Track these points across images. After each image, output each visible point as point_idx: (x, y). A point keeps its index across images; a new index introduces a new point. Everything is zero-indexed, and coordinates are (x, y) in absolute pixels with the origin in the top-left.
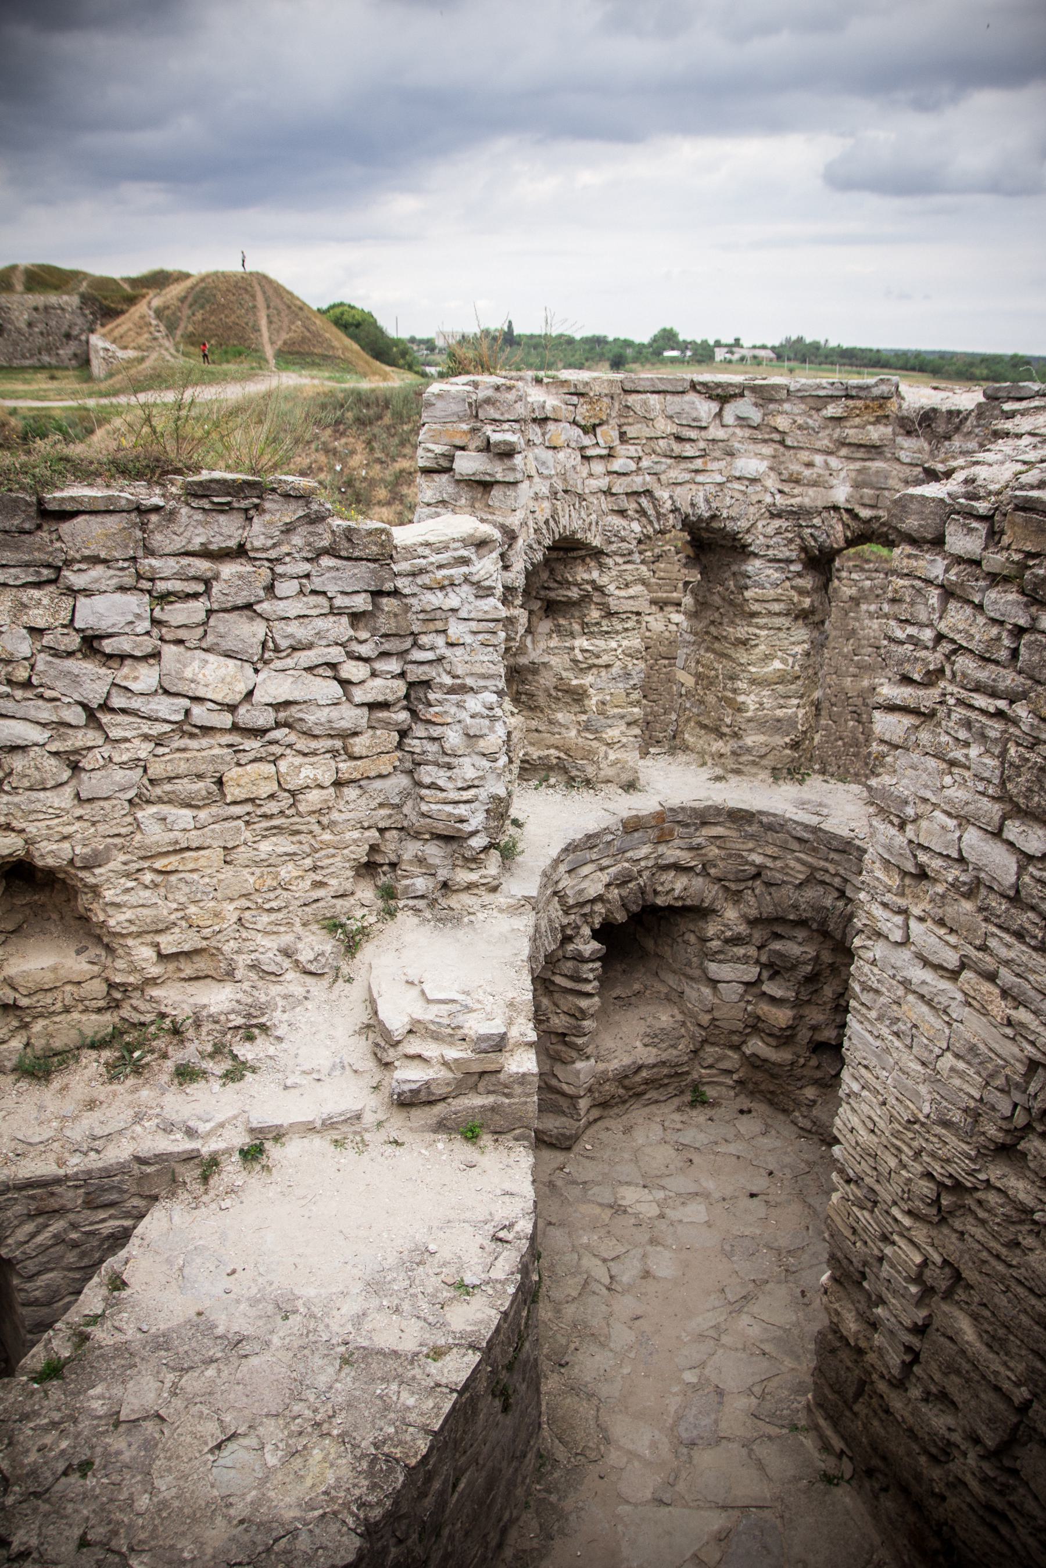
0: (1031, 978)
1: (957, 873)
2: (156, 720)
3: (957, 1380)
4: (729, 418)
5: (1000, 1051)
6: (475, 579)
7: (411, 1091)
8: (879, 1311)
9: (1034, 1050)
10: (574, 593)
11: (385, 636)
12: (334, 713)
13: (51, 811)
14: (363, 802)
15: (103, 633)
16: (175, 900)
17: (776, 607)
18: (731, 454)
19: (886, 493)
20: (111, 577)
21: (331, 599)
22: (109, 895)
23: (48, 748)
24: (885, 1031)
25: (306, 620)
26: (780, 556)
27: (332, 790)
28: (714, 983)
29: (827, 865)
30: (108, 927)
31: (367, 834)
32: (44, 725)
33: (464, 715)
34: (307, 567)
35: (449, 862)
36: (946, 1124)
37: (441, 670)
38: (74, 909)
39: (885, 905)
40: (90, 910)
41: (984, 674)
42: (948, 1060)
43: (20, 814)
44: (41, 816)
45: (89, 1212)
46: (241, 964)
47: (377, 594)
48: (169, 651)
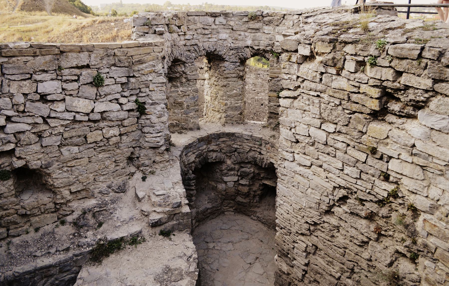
0: (332, 165)
1: (309, 140)
2: (65, 120)
3: (319, 275)
4: (217, 23)
5: (324, 186)
6: (156, 71)
7: (155, 222)
8: (294, 262)
9: (335, 184)
10: (178, 75)
11: (132, 89)
12: (118, 114)
13: (34, 151)
14: (128, 139)
15: (47, 94)
16: (74, 175)
17: (234, 75)
18: (218, 33)
19: (261, 42)
20: (49, 76)
21: (115, 79)
22: (54, 176)
23: (31, 131)
24: (290, 186)
25: (108, 86)
26: (234, 61)
27: (119, 137)
28: (226, 183)
29: (255, 146)
30: (54, 186)
31: (130, 149)
32: (29, 124)
33: (156, 111)
34: (107, 70)
35: (155, 155)
36: (310, 208)
37: (148, 98)
38: (387, 102)
39: (287, 151)
40: (47, 181)
41: (313, 85)
42: (310, 190)
43: (24, 153)
44: (31, 153)
45: (61, 274)
46: (96, 192)
47: (128, 77)
48: (67, 98)
